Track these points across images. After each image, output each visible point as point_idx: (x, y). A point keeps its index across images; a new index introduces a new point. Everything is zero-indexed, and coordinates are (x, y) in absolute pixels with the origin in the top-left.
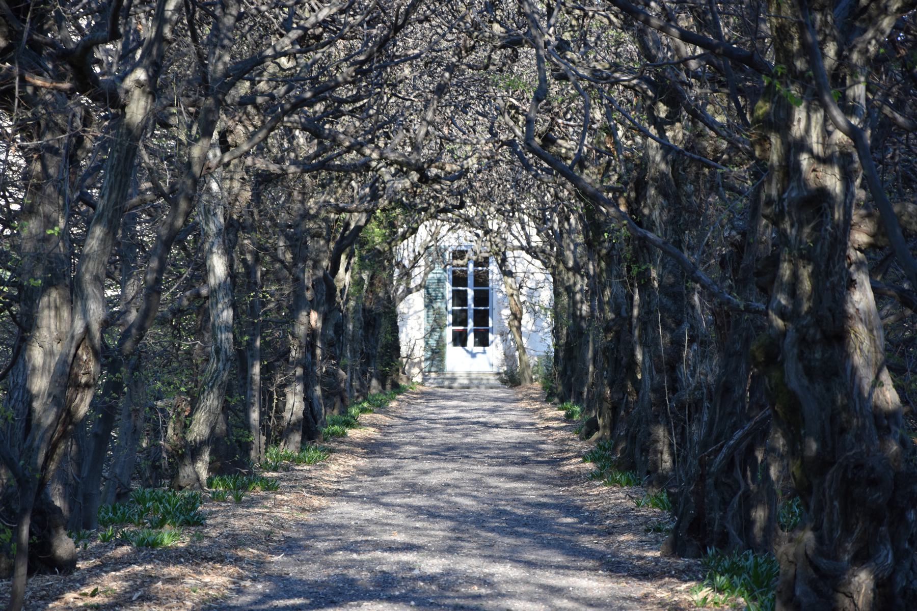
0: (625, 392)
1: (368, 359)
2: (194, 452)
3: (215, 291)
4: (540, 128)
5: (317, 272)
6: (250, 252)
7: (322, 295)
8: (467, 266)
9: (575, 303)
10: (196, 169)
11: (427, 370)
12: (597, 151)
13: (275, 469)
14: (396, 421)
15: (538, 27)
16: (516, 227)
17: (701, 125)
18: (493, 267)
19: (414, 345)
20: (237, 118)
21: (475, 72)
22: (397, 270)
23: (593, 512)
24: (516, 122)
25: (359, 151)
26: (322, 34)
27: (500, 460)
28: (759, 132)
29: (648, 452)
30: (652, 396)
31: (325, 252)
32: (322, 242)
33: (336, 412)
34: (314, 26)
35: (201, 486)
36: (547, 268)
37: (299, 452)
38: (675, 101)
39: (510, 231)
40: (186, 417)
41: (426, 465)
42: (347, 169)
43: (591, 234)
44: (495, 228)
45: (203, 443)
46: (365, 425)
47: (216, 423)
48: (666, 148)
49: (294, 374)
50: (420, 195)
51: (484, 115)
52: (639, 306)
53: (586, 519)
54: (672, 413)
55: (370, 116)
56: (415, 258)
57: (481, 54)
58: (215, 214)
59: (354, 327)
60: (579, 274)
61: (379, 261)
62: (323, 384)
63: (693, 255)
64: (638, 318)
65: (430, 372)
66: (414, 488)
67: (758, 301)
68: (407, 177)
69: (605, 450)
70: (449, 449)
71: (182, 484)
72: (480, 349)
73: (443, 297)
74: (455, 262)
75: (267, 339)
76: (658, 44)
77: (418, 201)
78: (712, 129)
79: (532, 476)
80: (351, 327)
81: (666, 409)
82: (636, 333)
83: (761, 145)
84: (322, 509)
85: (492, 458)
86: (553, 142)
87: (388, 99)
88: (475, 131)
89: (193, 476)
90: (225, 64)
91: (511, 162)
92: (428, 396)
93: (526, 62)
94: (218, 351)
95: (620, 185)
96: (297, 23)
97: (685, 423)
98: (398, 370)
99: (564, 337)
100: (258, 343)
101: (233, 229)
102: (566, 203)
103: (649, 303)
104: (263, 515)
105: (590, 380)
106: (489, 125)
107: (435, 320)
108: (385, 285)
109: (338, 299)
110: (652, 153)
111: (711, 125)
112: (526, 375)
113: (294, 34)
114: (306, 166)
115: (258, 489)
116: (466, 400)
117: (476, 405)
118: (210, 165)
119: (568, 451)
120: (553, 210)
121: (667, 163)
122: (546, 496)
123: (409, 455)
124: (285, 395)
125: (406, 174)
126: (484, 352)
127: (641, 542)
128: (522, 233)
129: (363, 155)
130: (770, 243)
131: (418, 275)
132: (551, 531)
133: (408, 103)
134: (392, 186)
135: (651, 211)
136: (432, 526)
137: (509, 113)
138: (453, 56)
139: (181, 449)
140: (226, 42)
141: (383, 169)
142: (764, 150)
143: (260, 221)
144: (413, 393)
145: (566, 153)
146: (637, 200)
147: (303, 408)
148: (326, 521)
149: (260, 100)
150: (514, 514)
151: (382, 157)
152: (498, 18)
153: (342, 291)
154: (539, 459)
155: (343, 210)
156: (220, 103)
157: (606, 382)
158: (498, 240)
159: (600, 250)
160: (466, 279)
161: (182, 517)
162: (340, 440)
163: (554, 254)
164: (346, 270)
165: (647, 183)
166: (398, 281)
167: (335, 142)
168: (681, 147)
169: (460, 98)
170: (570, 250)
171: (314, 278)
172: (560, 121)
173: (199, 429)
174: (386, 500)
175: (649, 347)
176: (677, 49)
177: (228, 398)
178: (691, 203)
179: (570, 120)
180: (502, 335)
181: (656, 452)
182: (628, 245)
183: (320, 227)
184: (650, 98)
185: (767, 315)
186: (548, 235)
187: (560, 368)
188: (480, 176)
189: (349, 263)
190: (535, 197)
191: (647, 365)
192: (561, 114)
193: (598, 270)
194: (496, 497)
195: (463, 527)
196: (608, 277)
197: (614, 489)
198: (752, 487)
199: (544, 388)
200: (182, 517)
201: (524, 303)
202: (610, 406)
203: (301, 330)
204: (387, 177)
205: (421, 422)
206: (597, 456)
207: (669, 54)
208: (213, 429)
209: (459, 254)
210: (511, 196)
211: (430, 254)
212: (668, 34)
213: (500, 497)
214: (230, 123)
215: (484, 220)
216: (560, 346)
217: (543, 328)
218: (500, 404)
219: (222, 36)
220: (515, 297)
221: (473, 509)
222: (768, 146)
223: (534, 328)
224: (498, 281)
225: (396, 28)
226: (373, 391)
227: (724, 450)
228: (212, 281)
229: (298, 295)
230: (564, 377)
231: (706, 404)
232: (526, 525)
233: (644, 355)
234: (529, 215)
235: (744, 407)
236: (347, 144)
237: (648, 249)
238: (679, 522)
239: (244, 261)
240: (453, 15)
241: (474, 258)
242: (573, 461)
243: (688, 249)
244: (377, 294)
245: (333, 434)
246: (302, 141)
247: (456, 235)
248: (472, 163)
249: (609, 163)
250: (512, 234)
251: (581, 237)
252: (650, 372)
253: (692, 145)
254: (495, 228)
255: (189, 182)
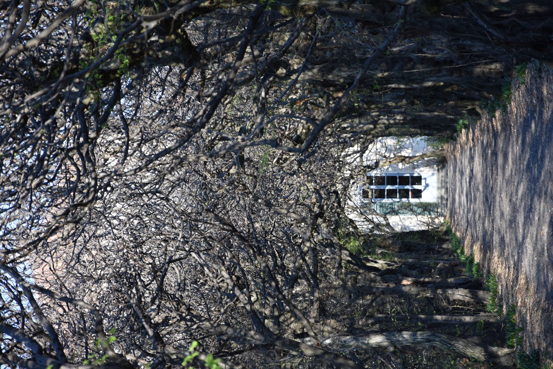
0: (452, 92)
1: (430, 250)
2: (492, 357)
3: (391, 342)
4: (291, 145)
5: (378, 280)
6: (367, 320)
7: (391, 277)
8: (372, 190)
9: (396, 124)
10: (319, 352)
11: (436, 214)
12: (305, 111)
13: (501, 307)
14: (469, 232)
15: (233, 146)
16: (349, 160)
17: (291, 48)
18: (373, 173)
19: (420, 221)
20: (286, 328)
21: (258, 184)
22: (375, 232)
23: (528, 111)
24: (286, 160)
25: (306, 254)
26: (236, 276)
27: (494, 168)
28: (298, 12)
29: (490, 78)
30: (455, 75)
31: (365, 275)
32: (360, 277)
33: (464, 270)
34: (232, 280)
35: (513, 352)
36: (374, 141)
37: (490, 292)
38: (276, 63)
39: (351, 163)
40: (470, 361)
41: (497, 214)
42: (316, 262)
43: (354, 114)
44: (349, 172)
45: (486, 351)
46: (472, 251)
47: (473, 342)
48: (304, 68)
49: (441, 294)
50: (330, 217)
51: (282, 179)
52: (399, 84)
53: (532, 115)
54: (466, 63)
55: (284, 247)
56: (367, 221)
57: (248, 181)
58: (345, 341)
59: (411, 258)
60: (378, 121)
61: (370, 242)
62: (447, 277)
63: (368, 52)
64: (406, 85)
65: (437, 212)
66: (513, 221)
67: (398, 12)
68: (320, 225)
69: (487, 104)
70: (487, 200)
71: (512, 364)
72: (423, 181)
73: (391, 204)
74: (370, 196)
75: (420, 311)
76: (243, 74)
77: (333, 219)
78: (293, 41)
79: (504, 149)
80: (410, 260)
81: (463, 67)
82: (415, 86)
83: (306, 11)
84: (527, 278)
85: (492, 173)
86: (299, 137)
87: (274, 236)
88: (292, 184)
89: (507, 357)
90: (255, 334)
91: (310, 163)
92: (453, 213)
93: (252, 154)
94: (428, 341)
95: (326, 96)
96: (230, 291)
97: (472, 55)
98: (437, 232)
99: (416, 130)
100: (422, 316)
101: (352, 331)
102: (334, 129)
103: (397, 78)
104: (531, 314)
105: (443, 114)
106: (288, 176)
107: (406, 209)
108: (385, 239)
109: (394, 267)
110: (307, 77)
111: (291, 42)
112: (439, 153)
113: (237, 292)
114: (314, 287)
115: (514, 317)
116: (455, 190)
117: (458, 184)
118: (316, 343)
119: (488, 127)
120: (339, 137)
121: (313, 68)
122: (517, 140)
123: (491, 224)
124: (454, 300)
125: (318, 226)
126: (425, 179)
127: (547, 81)
128: (352, 156)
129: (308, 251)
130: (363, 5)
131: (377, 219)
132: (540, 137)
133: (276, 225)
134: (326, 234)
135: (342, 77)
136: (537, 210)
137: (282, 164)
138: (249, 197)
139: (490, 364)
140: (243, 333)
141: (315, 240)
142: (309, 9)
143: (348, 315)
144: (451, 223)
145: (305, 129)
146: (335, 86)
147: (462, 289)
148: (534, 275)
149: (276, 313)
150: (529, 159)
151: (309, 240)
152: (226, 170)
153: (389, 265)
154: (493, 144)
155: (340, 264)
156: (279, 337)
157: (445, 104)
158: (357, 170)
159: (364, 108)
160: (380, 190)
161: (534, 364)
162: (481, 267)
163: (365, 136)
164: (376, 262)
165: (325, 80)
166: (381, 231)
167: (300, 268)
168: (304, 60)
169: (273, 193)
170: (363, 127)
171: (381, 282)
172: (287, 133)
173: (477, 353)
174: (520, 238)
175: (424, 78)
176: (247, 62)
177: (457, 335)
178: (338, 53)
179: (286, 127)
180: (414, 168)
181: (490, 73)
182: (362, 91)
183: (351, 278)
184: (274, 79)
185: (408, 5)
186: (354, 140)
187: (435, 132)
188: (318, 181)
189: (372, 261)
190: (331, 148)
191: (435, 79)
192: (282, 132)
193: (376, 110)
194: (518, 171)
195: (538, 190)
196: (381, 103)
197: (513, 98)
198: (514, 13)
199: (447, 142)
200: (534, 364)
201: (394, 155)
202: (460, 102)
203: (414, 290)
204: (320, 237)
205: (469, 217)
206: (491, 109)
207: (248, 67)
208: (477, 345)
209: (365, 194)
210: (330, 163)
211: (365, 212)
212: (238, 68)
213: (518, 168)
214: (289, 331)
215: (344, 179)
216: (422, 132)
217: (410, 143)
218: (457, 169)
219: (239, 335)
220: (391, 160)
221: (526, 184)
222: (307, 7)
223: (410, 149)
224: (381, 170)
225: (234, 230)
226: (450, 246)
227: (490, 30)
228: (385, 344)
229: (392, 292)
230: (440, 130)
231: (461, 42)
232: (536, 152)
233: (429, 81)
234: (342, 151)
235: (464, 19)
236: (301, 261)
237: (365, 79)
238: (535, 57)
239: (373, 324)
240: (225, 197)
241: (367, 185)
242: (494, 123)
243: (365, 54)
244: (390, 244)
245: (478, 271)
246: (298, 289)
247: (354, 196)
248: (311, 186)
249: (312, 103)
250: (353, 162)
251: (355, 120)
252: (440, 77)
253: (302, 53)
254: (349, 172)
255: (327, 356)
